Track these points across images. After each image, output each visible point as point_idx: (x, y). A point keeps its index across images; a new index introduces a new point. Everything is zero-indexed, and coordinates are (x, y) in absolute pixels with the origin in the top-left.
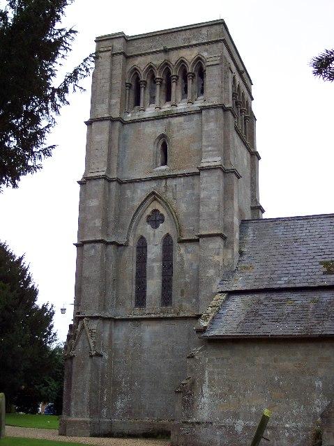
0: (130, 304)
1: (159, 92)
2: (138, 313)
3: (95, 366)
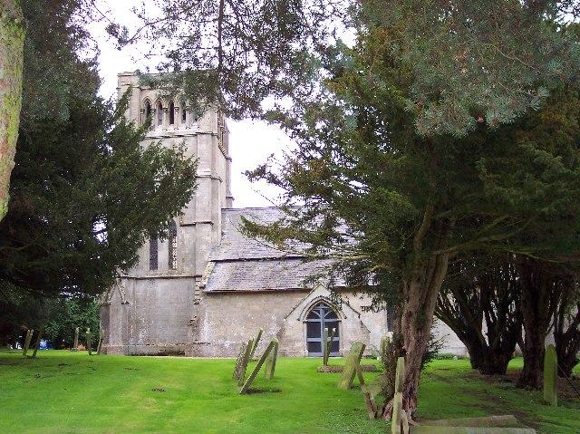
0: (147, 267)
1: (165, 116)
2: (151, 274)
3: (125, 309)
